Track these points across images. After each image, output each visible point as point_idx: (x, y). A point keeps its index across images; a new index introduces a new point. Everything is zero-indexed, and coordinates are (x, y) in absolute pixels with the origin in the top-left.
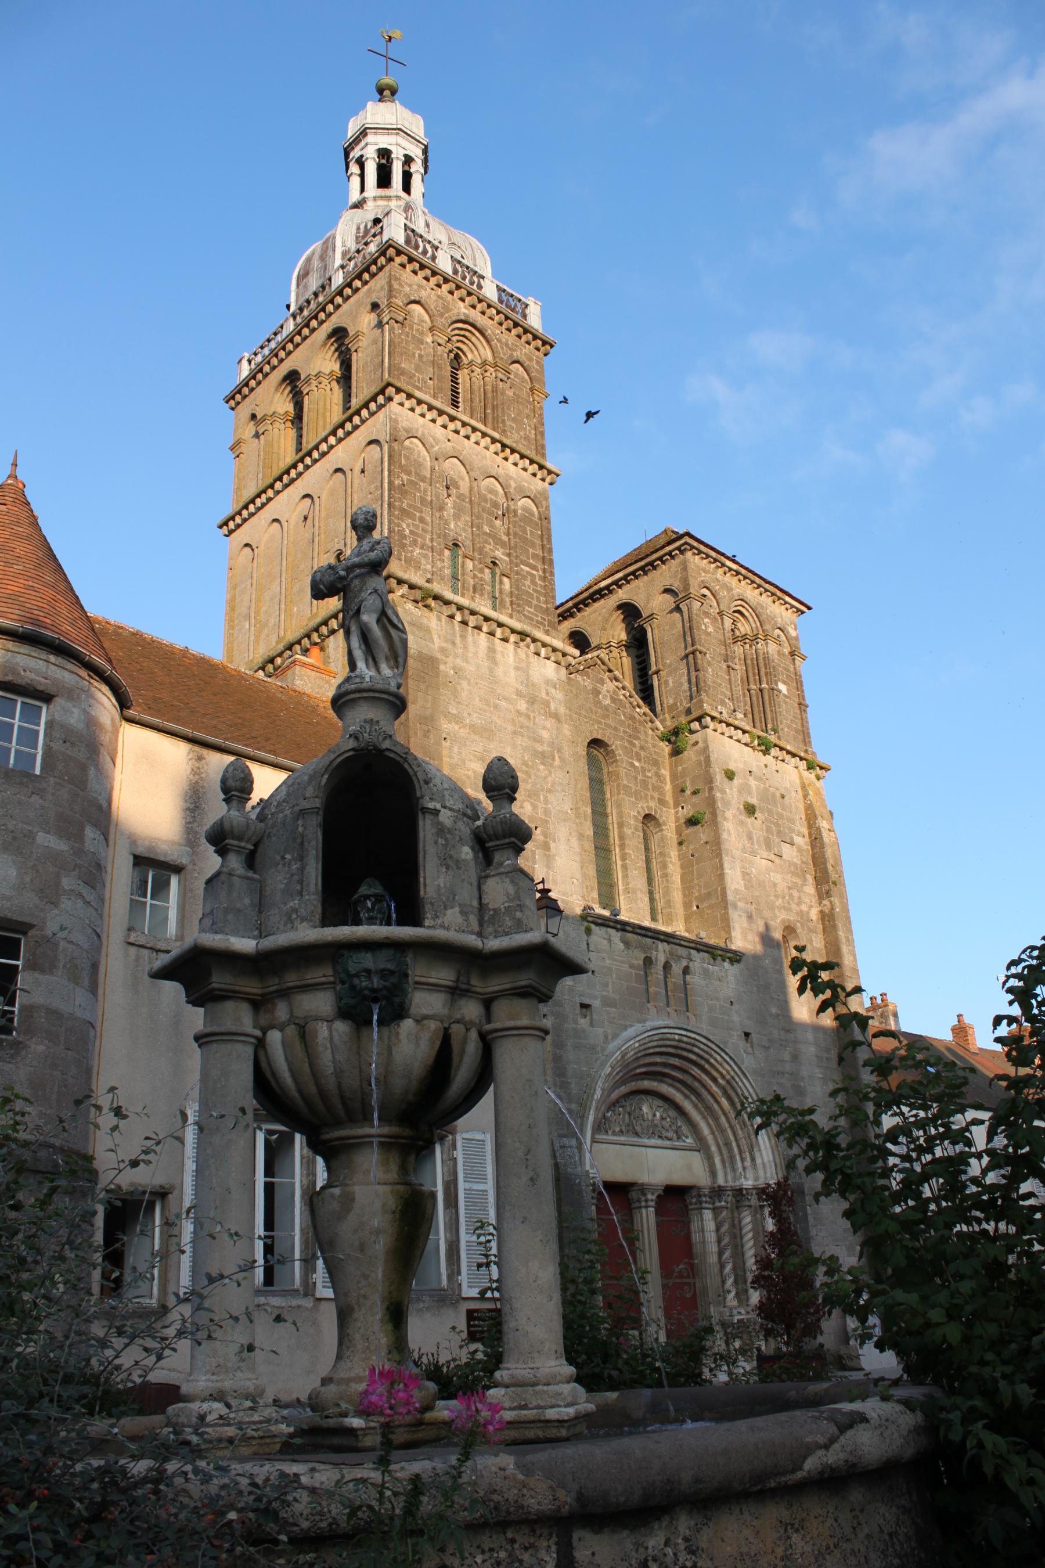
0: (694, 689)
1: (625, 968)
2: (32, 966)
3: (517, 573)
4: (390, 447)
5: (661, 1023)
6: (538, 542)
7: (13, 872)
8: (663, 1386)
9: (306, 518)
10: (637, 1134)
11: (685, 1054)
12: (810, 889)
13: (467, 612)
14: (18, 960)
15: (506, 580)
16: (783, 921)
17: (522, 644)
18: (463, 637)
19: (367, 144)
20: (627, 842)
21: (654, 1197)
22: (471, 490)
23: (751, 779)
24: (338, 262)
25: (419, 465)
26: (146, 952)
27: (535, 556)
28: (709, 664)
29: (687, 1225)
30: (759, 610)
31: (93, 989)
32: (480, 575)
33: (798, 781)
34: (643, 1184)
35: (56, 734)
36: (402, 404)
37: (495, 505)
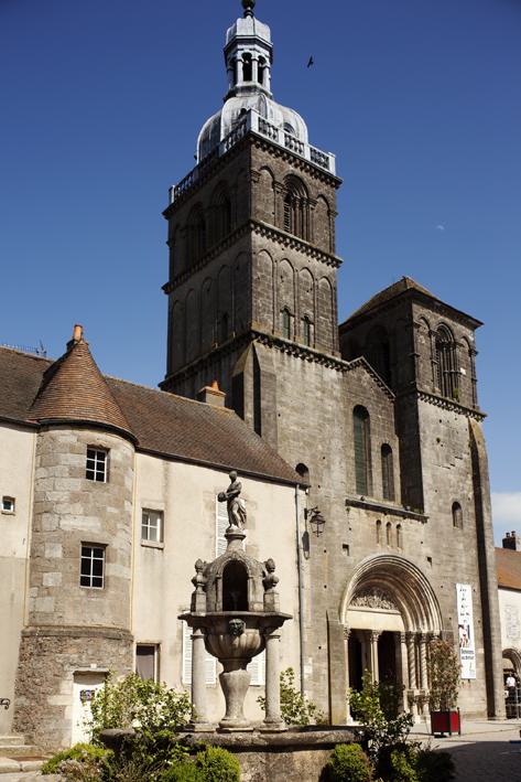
1: (367, 527)
6: (330, 303)
7: (99, 524)
8: (93, 479)
12: (470, 482)
15: (312, 326)
18: (289, 361)
24: (222, 138)
27: (328, 311)
37: (307, 283)
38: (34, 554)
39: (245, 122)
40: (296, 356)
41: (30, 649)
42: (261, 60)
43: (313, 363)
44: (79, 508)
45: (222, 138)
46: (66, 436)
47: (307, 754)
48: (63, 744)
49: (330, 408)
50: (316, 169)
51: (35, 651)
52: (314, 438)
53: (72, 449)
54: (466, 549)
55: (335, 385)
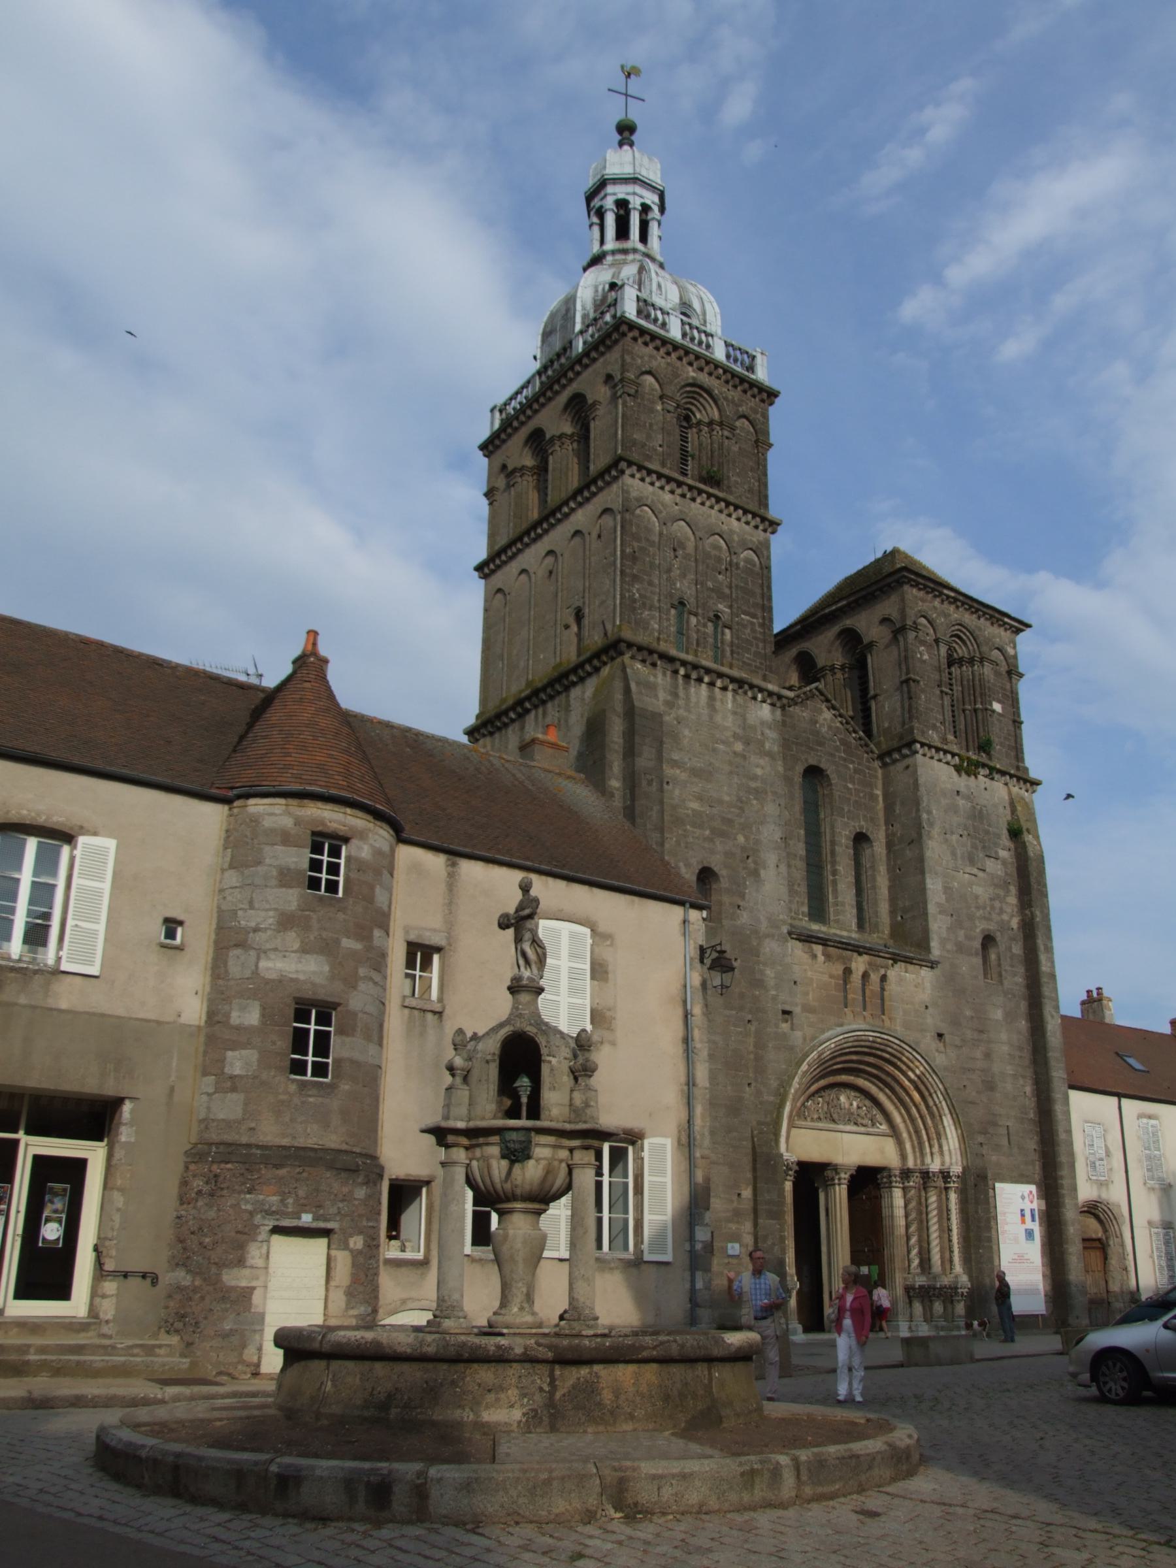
0: (907, 715)
1: (825, 978)
2: (341, 1031)
3: (738, 623)
4: (622, 518)
5: (854, 1027)
6: (758, 591)
7: (327, 968)
9: (551, 572)
10: (834, 1121)
11: (879, 1053)
12: (1013, 900)
13: (689, 667)
14: (330, 1026)
15: (727, 631)
16: (983, 930)
17: (740, 691)
19: (605, 196)
20: (838, 859)
21: (847, 1176)
22: (696, 548)
23: (958, 798)
24: (578, 327)
25: (649, 530)
26: (416, 1012)
28: (923, 691)
29: (878, 1198)
30: (977, 632)
31: (380, 1044)
32: (702, 629)
33: (1007, 798)
34: (836, 1165)
35: (353, 866)
36: (633, 476)
37: (719, 560)
38: (213, 1017)
39: (615, 303)
40: (700, 680)
41: (198, 1183)
42: (645, 209)
43: (730, 694)
44: (292, 939)
45: (578, 327)
46: (270, 812)
47: (624, 1373)
48: (245, 1357)
49: (759, 772)
50: (734, 375)
51: (206, 1189)
52: (729, 822)
53: (286, 839)
54: (1010, 1016)
55: (767, 731)
